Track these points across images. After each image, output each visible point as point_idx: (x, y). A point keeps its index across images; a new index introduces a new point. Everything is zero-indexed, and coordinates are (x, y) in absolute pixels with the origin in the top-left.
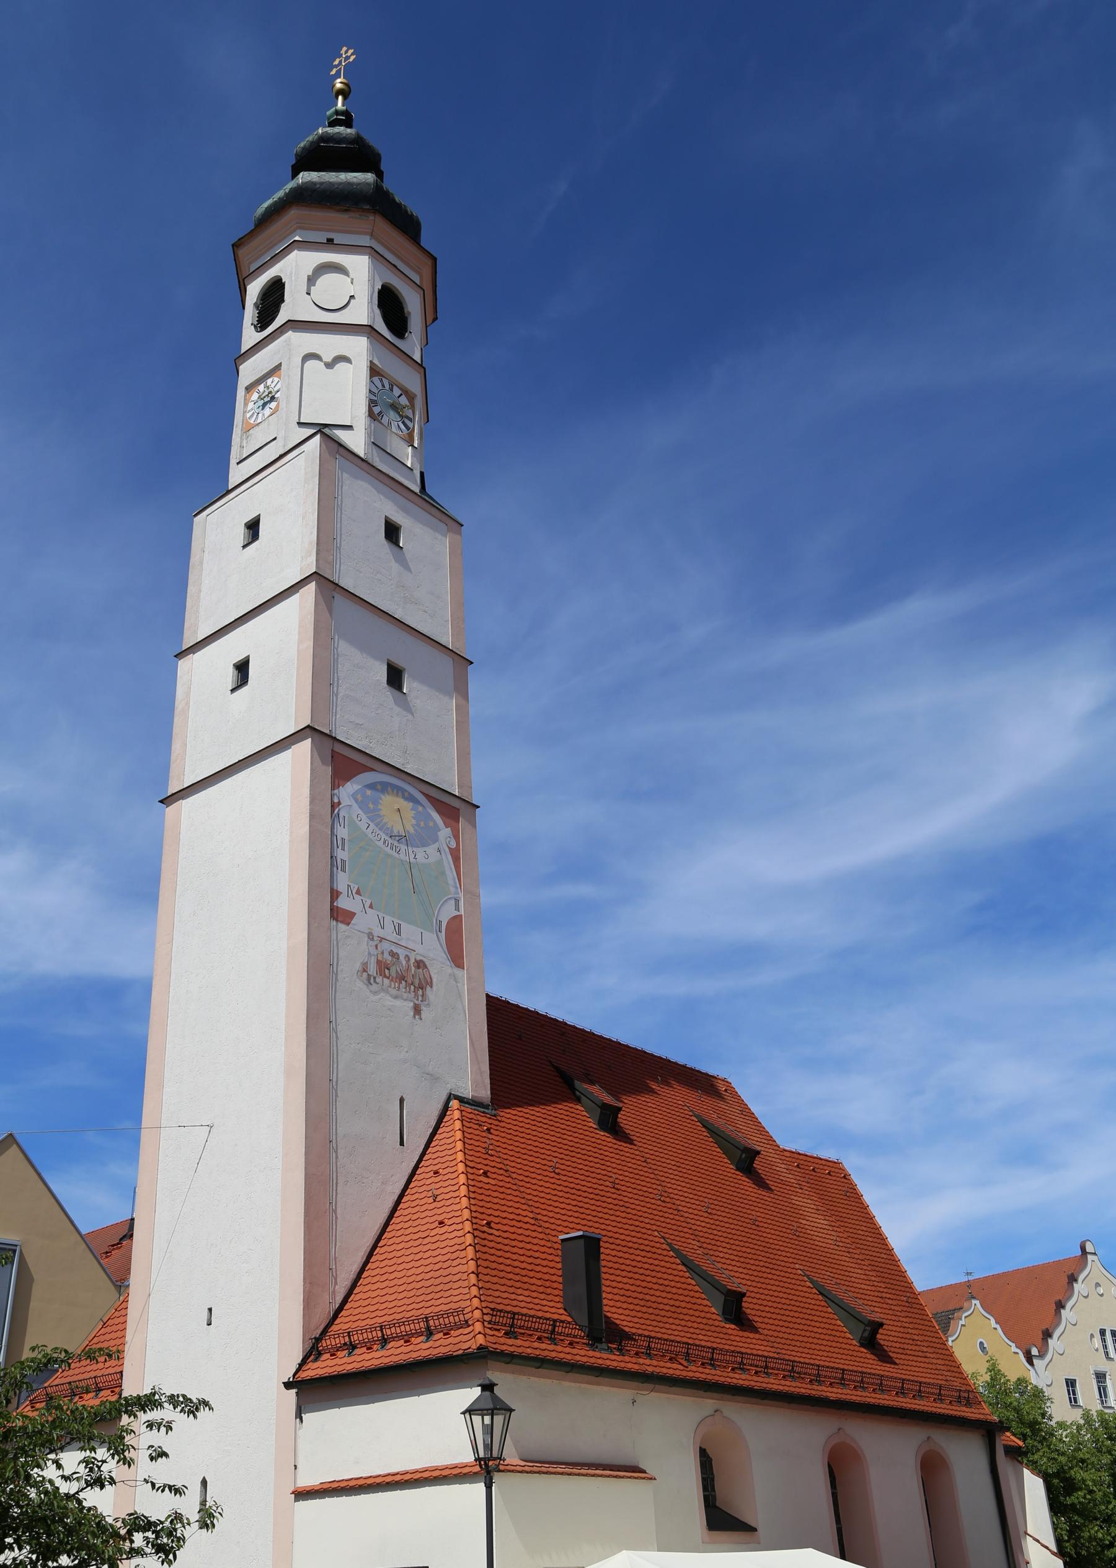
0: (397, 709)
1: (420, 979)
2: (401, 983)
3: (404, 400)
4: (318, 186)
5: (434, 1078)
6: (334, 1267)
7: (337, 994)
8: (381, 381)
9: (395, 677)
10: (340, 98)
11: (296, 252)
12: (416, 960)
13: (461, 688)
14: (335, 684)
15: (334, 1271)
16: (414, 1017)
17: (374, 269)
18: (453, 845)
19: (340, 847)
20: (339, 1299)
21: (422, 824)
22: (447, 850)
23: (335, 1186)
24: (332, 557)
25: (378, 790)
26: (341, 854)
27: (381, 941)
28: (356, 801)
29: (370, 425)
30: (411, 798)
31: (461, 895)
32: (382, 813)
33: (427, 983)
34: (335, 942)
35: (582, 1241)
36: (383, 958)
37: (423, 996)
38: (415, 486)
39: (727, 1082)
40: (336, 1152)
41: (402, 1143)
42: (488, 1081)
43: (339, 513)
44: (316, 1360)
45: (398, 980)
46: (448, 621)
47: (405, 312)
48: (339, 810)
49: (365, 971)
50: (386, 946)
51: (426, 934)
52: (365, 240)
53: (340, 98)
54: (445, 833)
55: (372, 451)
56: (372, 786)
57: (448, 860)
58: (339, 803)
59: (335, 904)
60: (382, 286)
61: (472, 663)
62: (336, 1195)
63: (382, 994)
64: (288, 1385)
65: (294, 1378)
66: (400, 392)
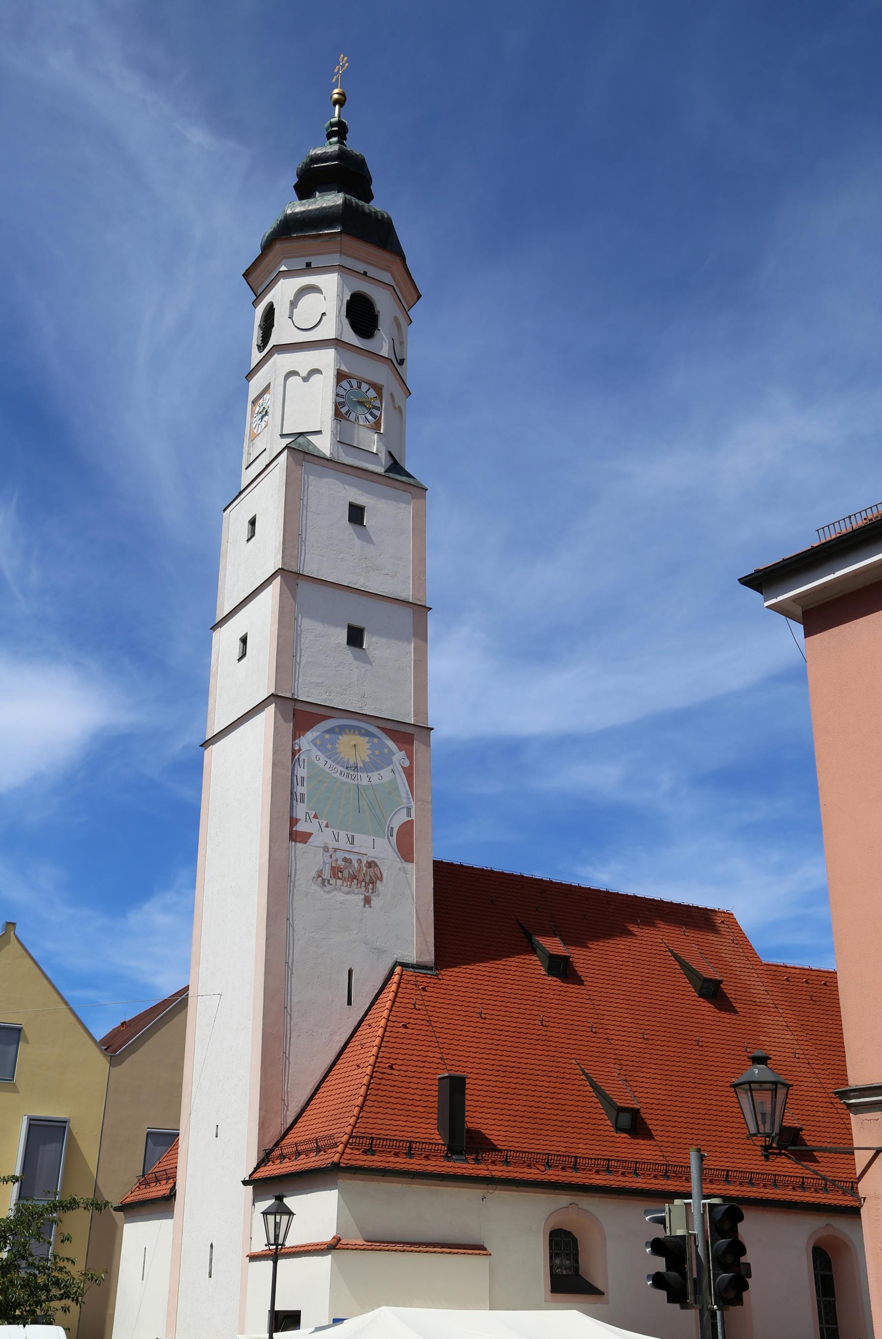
0: (356, 663)
1: (370, 876)
2: (352, 881)
3: (372, 393)
4: (299, 216)
5: (381, 951)
6: (286, 1098)
7: (294, 897)
8: (349, 382)
9: (355, 637)
10: (337, 107)
11: (282, 280)
12: (367, 862)
13: (420, 633)
14: (298, 655)
15: (286, 1101)
16: (364, 906)
17: (343, 283)
18: (407, 764)
19: (300, 784)
20: (290, 1121)
21: (377, 753)
22: (401, 769)
23: (288, 1039)
24: (297, 551)
25: (336, 733)
26: (299, 790)
27: (335, 852)
28: (316, 745)
29: (336, 427)
30: (368, 734)
31: (413, 804)
32: (339, 750)
33: (378, 878)
34: (293, 859)
35: (448, 1080)
36: (337, 864)
37: (373, 889)
38: (379, 468)
39: (728, 913)
40: (290, 1015)
41: (349, 1003)
42: (432, 948)
43: (305, 512)
44: (265, 1165)
45: (350, 880)
46: (409, 577)
47: (376, 310)
48: (299, 756)
49: (319, 876)
50: (340, 855)
51: (378, 841)
52: (335, 259)
53: (337, 107)
54: (399, 756)
55: (338, 449)
56: (330, 731)
57: (402, 778)
58: (300, 750)
59: (294, 829)
60: (352, 296)
61: (431, 609)
62: (290, 1047)
63: (335, 892)
64: (245, 1183)
65: (249, 1178)
66: (368, 387)
